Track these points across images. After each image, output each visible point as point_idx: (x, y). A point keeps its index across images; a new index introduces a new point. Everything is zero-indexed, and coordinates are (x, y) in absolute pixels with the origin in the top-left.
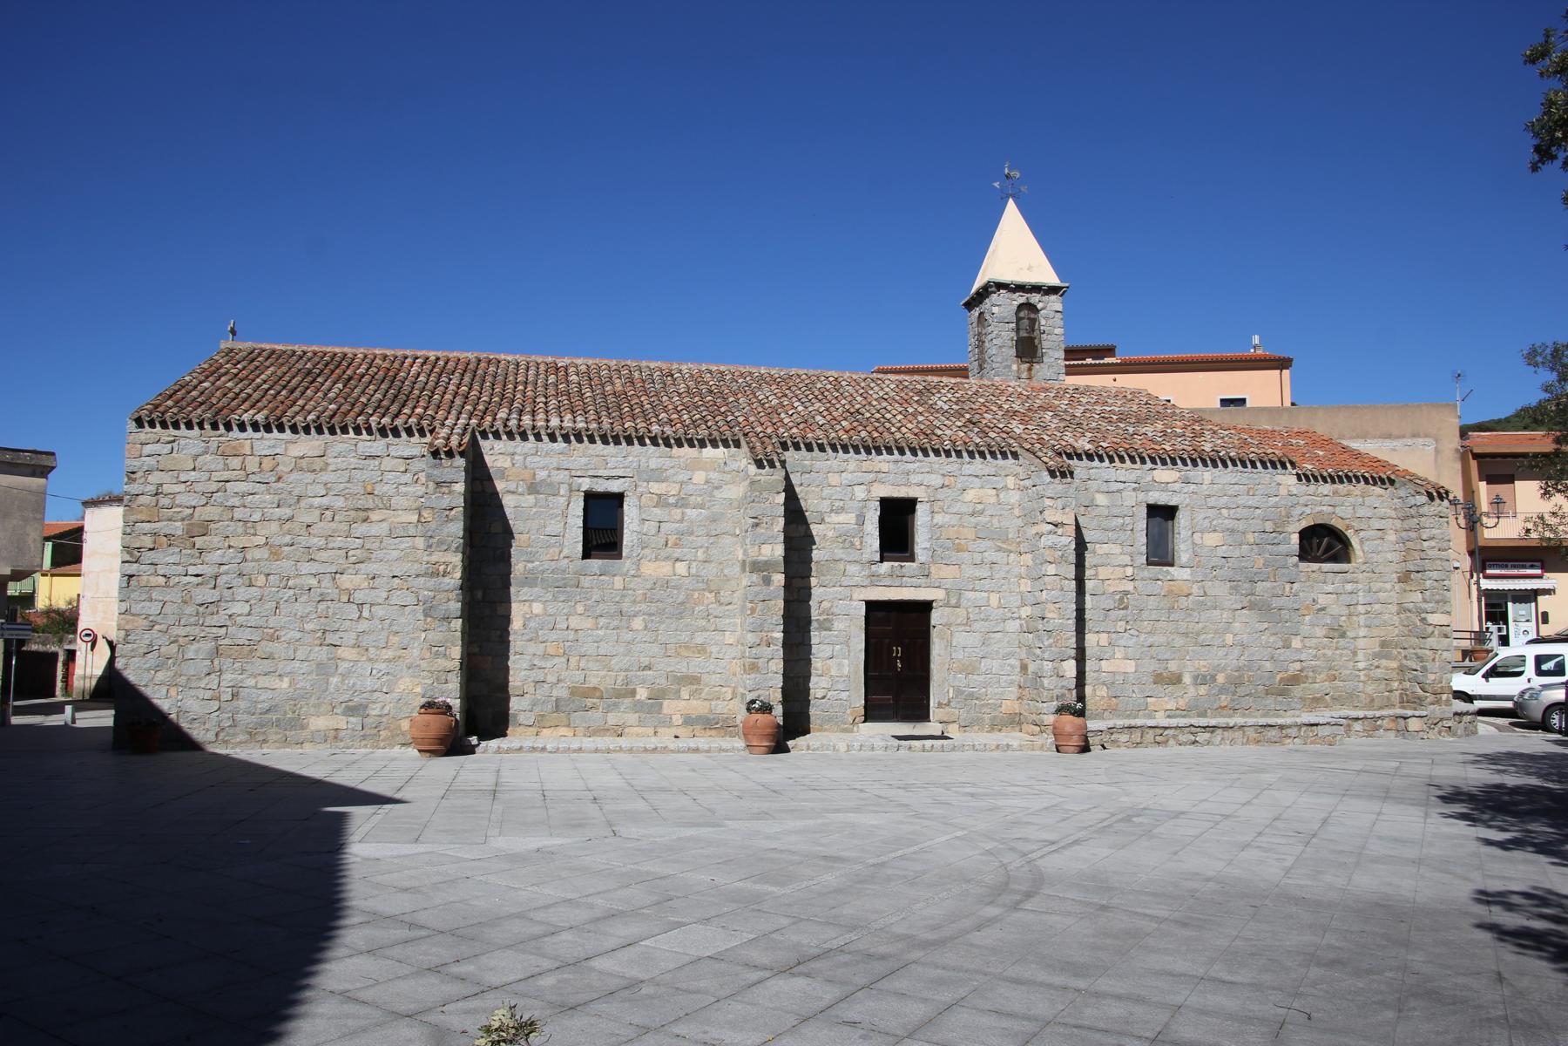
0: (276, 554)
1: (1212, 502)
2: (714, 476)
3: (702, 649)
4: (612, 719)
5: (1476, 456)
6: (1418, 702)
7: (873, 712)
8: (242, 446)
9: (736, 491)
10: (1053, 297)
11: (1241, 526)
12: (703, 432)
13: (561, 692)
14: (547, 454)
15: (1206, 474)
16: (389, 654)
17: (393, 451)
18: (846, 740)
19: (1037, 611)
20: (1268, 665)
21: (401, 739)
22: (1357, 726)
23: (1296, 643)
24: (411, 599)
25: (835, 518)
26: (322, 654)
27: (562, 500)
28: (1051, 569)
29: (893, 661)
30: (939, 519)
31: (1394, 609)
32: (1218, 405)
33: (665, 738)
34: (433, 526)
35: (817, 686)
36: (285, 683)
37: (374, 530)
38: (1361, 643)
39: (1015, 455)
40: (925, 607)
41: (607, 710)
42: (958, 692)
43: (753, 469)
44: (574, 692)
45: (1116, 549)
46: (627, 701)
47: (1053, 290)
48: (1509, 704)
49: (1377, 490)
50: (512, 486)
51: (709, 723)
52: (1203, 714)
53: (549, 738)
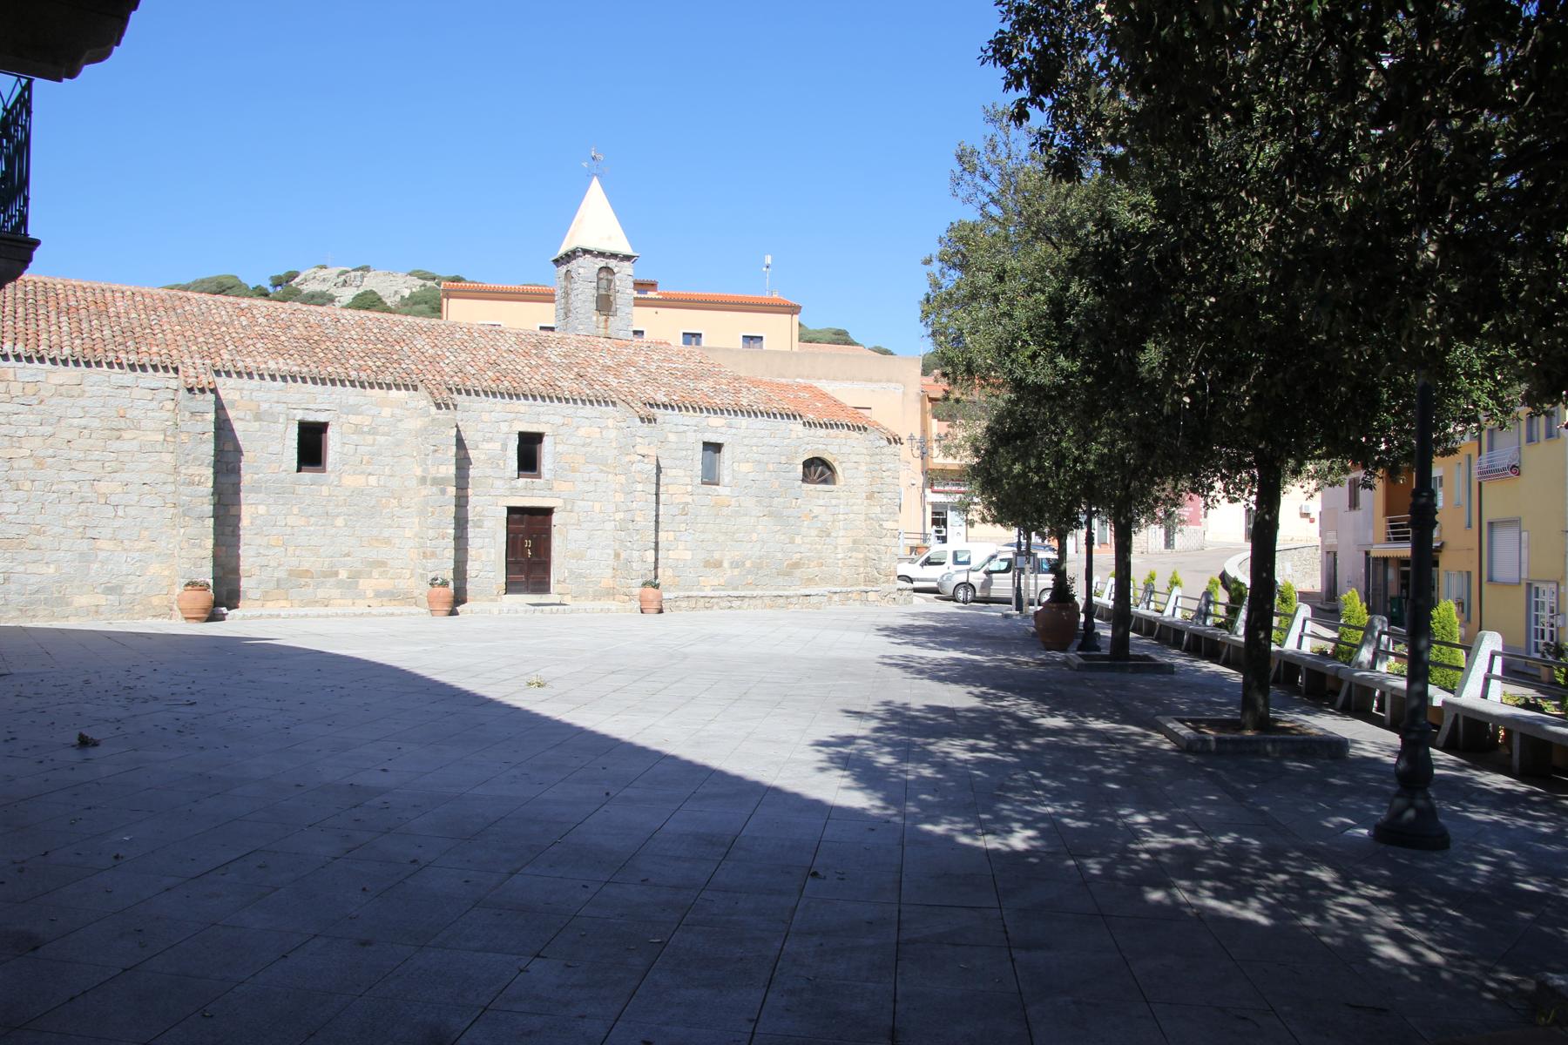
0: (40, 464)
1: (746, 441)
2: (397, 411)
3: (388, 541)
4: (321, 593)
5: (931, 400)
6: (875, 581)
7: (511, 587)
8: (6, 373)
9: (416, 424)
10: (626, 264)
11: (765, 458)
12: (389, 379)
13: (281, 574)
14: (269, 390)
15: (743, 422)
16: (141, 545)
17: (142, 383)
18: (495, 607)
19: (629, 516)
20: (779, 555)
21: (152, 612)
22: (836, 598)
23: (798, 540)
24: (158, 502)
25: (486, 446)
26: (84, 545)
27: (281, 427)
28: (640, 487)
29: (524, 550)
30: (560, 448)
31: (863, 517)
32: (739, 343)
33: (361, 607)
34: (189, 446)
35: (472, 568)
36: (52, 569)
37: (126, 446)
38: (840, 541)
39: (614, 404)
40: (547, 512)
41: (317, 586)
42: (571, 572)
43: (433, 409)
44: (291, 573)
45: (681, 473)
46: (332, 580)
47: (628, 258)
48: (934, 585)
49: (855, 434)
50: (241, 415)
51: (393, 596)
52: (735, 589)
53: (271, 607)
